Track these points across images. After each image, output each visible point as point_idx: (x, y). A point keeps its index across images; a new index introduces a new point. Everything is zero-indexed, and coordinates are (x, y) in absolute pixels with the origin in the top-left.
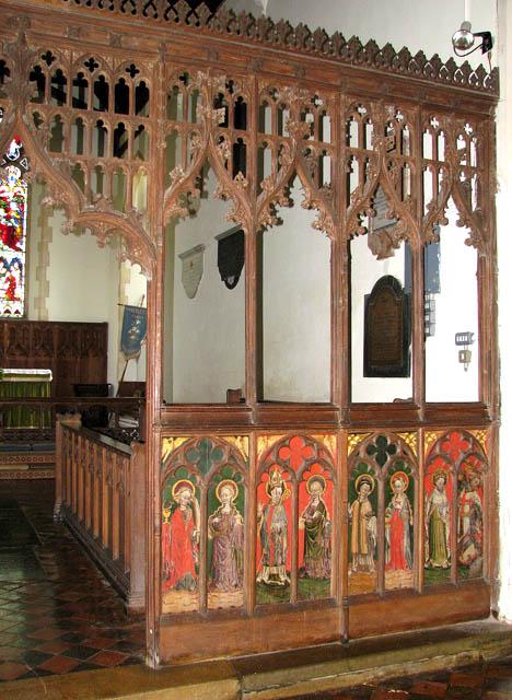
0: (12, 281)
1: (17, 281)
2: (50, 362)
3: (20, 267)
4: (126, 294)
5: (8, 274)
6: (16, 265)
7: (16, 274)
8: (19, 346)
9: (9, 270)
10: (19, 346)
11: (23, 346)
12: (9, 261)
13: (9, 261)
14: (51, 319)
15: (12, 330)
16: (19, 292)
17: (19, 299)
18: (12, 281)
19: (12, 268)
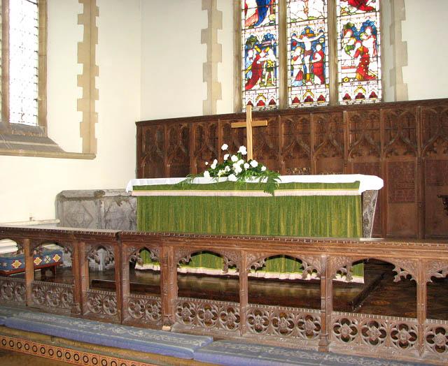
0: (364, 54)
1: (371, 52)
2: (378, 164)
3: (374, 33)
4: (96, 87)
5: (358, 45)
6: (368, 31)
7: (368, 44)
8: (365, 142)
9: (359, 40)
10: (365, 142)
11: (371, 141)
12: (358, 27)
13: (358, 27)
14: (413, 96)
15: (355, 120)
16: (374, 67)
17: (374, 78)
18: (364, 54)
19: (363, 37)
